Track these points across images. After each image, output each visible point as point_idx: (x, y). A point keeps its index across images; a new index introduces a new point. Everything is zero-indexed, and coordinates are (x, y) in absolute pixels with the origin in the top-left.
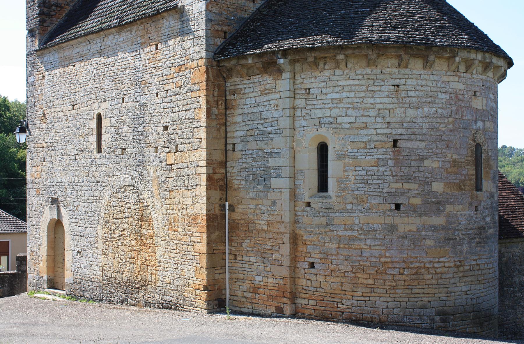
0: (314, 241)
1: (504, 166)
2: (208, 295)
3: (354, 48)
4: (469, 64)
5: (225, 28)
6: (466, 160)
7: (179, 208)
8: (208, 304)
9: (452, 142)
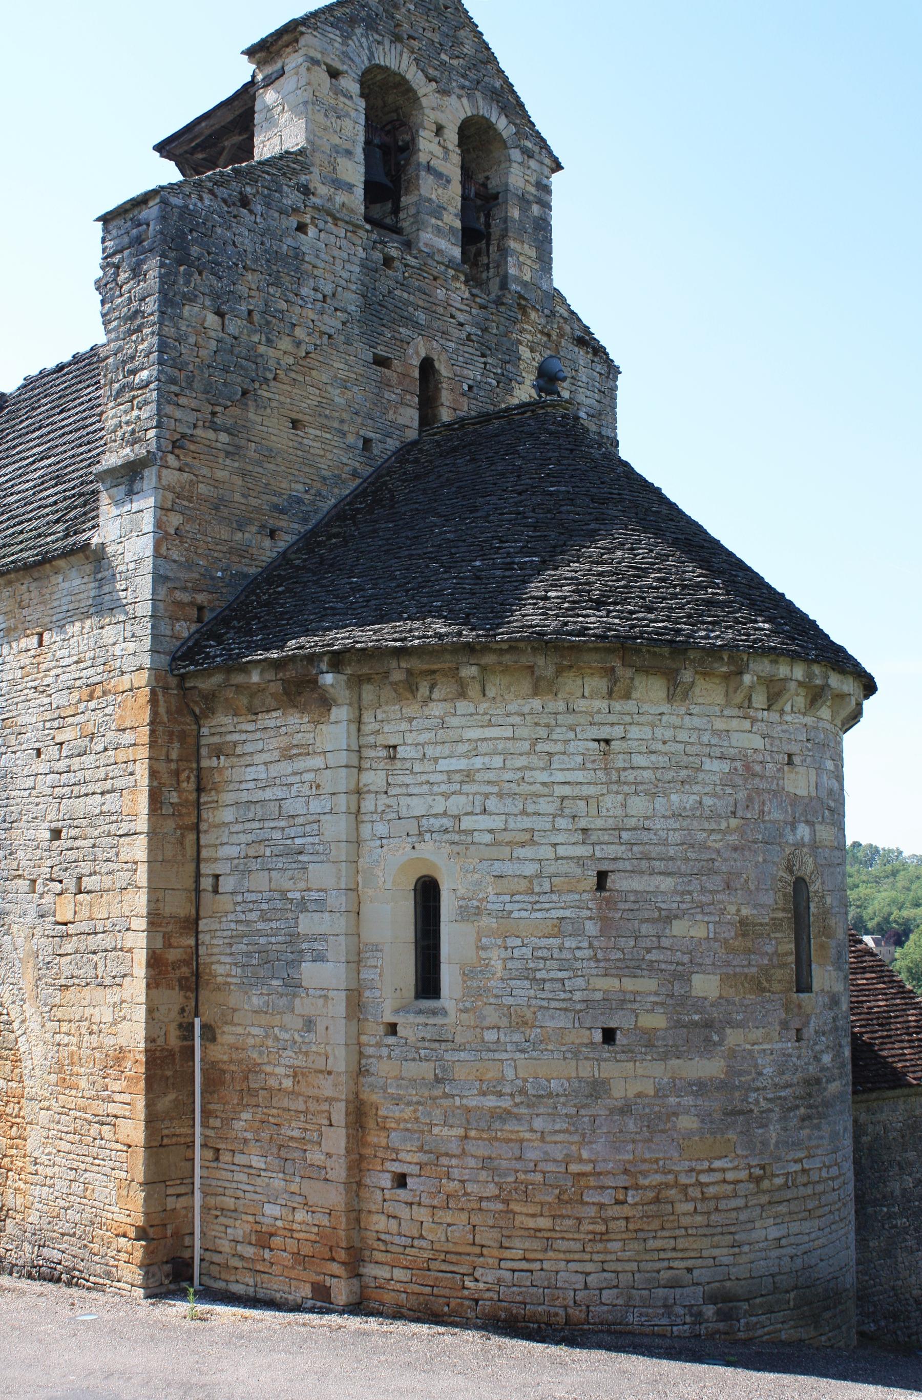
0: (405, 1121)
1: (858, 886)
2: (148, 1252)
3: (501, 650)
4: (776, 690)
5: (201, 598)
6: (773, 919)
7: (83, 1031)
8: (147, 1273)
9: (739, 875)
